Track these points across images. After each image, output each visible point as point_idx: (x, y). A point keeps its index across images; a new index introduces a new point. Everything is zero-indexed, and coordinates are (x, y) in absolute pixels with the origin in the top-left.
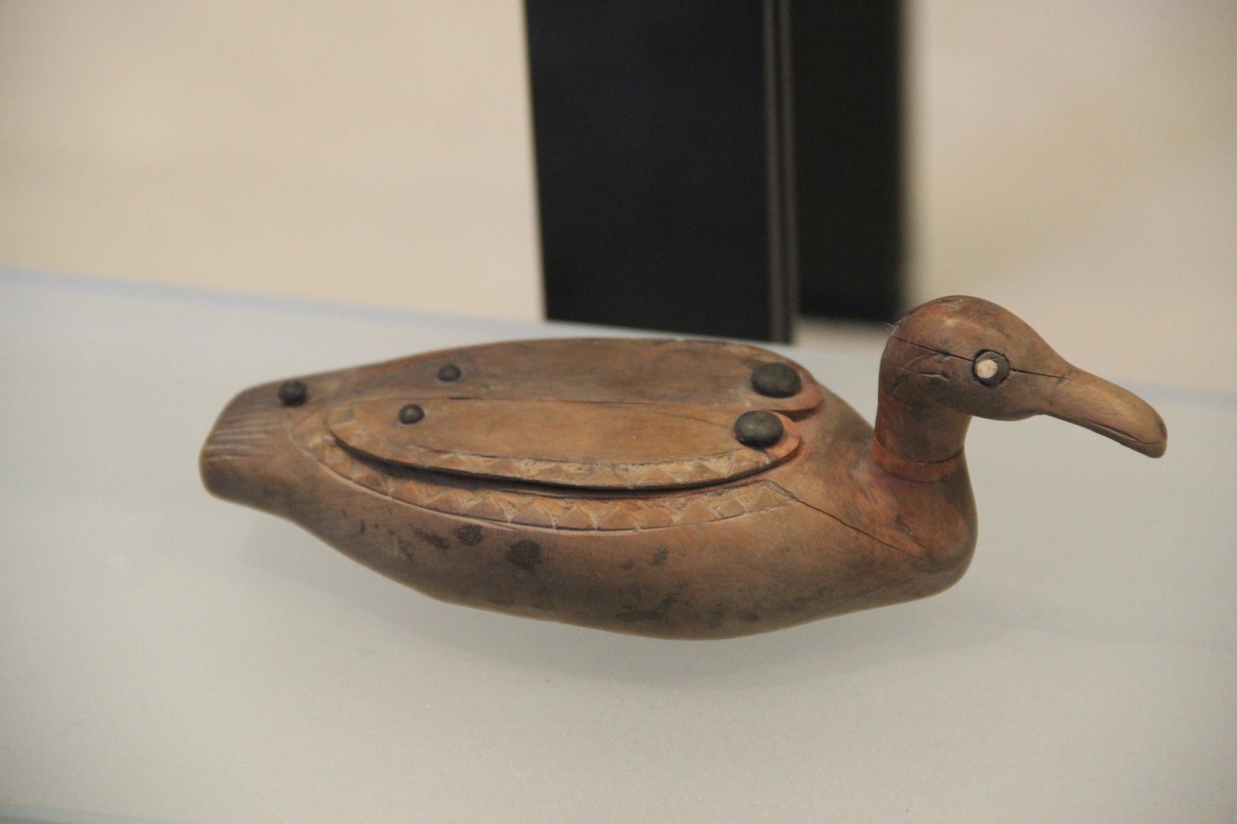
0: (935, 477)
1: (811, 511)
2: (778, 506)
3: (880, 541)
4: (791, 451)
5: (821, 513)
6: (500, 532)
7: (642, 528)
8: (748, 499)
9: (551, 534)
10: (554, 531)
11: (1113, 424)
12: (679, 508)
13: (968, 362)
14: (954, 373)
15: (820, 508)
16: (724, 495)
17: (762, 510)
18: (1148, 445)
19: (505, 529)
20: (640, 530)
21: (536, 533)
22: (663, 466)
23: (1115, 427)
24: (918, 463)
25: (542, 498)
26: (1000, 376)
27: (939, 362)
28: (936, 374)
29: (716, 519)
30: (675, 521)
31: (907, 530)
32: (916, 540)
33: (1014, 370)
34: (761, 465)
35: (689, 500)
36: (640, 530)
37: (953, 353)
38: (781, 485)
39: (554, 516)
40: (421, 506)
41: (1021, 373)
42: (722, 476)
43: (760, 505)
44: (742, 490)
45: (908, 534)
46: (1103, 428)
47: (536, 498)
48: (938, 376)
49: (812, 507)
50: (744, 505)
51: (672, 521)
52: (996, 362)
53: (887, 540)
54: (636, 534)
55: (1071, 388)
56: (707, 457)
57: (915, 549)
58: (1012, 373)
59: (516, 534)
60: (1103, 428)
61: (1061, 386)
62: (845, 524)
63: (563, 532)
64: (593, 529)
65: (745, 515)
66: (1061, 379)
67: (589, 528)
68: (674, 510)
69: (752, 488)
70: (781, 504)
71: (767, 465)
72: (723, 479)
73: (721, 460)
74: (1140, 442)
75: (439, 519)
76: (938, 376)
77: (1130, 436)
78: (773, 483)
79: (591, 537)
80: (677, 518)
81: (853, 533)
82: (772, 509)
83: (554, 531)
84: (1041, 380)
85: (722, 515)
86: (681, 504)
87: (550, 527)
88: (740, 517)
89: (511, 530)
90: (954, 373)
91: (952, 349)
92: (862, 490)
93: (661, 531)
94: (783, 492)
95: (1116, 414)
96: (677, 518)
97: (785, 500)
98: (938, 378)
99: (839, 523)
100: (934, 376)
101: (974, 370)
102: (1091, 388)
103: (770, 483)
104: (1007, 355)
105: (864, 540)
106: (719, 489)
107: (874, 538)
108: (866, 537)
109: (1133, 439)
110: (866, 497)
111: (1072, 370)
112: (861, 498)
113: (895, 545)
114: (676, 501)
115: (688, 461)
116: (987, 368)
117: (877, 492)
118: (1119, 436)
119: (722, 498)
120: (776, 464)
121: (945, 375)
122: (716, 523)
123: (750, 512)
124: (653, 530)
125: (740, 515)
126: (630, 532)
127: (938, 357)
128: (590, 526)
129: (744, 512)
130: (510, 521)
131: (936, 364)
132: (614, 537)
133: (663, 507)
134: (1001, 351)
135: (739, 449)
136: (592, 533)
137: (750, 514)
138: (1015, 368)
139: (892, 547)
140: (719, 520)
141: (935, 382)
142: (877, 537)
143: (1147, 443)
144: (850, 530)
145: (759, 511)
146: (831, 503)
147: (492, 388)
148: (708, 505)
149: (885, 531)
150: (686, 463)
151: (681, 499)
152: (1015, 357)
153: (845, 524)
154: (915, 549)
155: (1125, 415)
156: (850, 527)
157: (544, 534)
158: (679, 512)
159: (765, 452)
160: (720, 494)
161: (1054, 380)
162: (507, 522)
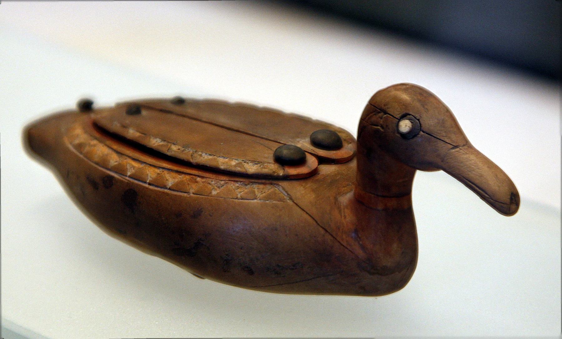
0: (380, 207)
2: (279, 201)
3: (339, 242)
5: (305, 213)
7: (193, 194)
10: (147, 186)
11: (477, 182)
12: (219, 187)
13: (396, 119)
14: (387, 126)
16: (249, 186)
18: (497, 203)
20: (192, 195)
21: (137, 185)
22: (221, 158)
23: (478, 185)
26: (413, 134)
27: (381, 118)
28: (378, 126)
29: (237, 198)
30: (213, 194)
31: (359, 240)
32: (363, 247)
33: (423, 132)
34: (276, 174)
35: (226, 183)
37: (390, 113)
40: (92, 162)
41: (427, 135)
43: (268, 198)
44: (261, 186)
45: (359, 243)
46: (470, 184)
48: (379, 127)
49: (300, 208)
50: (259, 195)
51: (211, 193)
52: (412, 122)
53: (345, 244)
54: (188, 196)
55: (461, 155)
56: (248, 161)
57: (361, 253)
58: (421, 133)
59: (129, 184)
60: (470, 184)
62: (319, 224)
63: (151, 187)
64: (166, 188)
65: (255, 201)
68: (216, 187)
69: (268, 187)
70: (281, 200)
73: (256, 165)
74: (492, 199)
76: (379, 127)
77: (486, 193)
78: (282, 187)
79: (164, 193)
80: (214, 193)
81: (322, 232)
82: (274, 202)
83: (147, 186)
84: (441, 144)
86: (221, 184)
87: (145, 182)
88: (252, 201)
90: (387, 126)
91: (389, 110)
92: (339, 208)
93: (203, 198)
95: (481, 176)
96: (214, 193)
98: (379, 129)
99: (314, 223)
100: (376, 127)
101: (398, 125)
102: (472, 157)
104: (420, 120)
105: (328, 238)
109: (487, 196)
111: (467, 143)
113: (349, 247)
114: (218, 182)
115: (235, 160)
116: (405, 126)
118: (479, 192)
119: (246, 187)
120: (287, 178)
122: (236, 200)
123: (260, 199)
124: (199, 196)
125: (253, 200)
126: (185, 195)
128: (165, 186)
129: (256, 199)
130: (128, 176)
131: (379, 119)
133: (210, 184)
134: (417, 116)
136: (166, 190)
137: (259, 201)
138: (424, 130)
139: (346, 248)
140: (238, 199)
142: (339, 239)
143: (496, 201)
144: (321, 229)
145: (266, 200)
149: (344, 237)
153: (319, 224)
154: (361, 253)
155: (493, 185)
156: (321, 227)
157: (141, 186)
158: (218, 189)
159: (284, 169)
162: (126, 176)
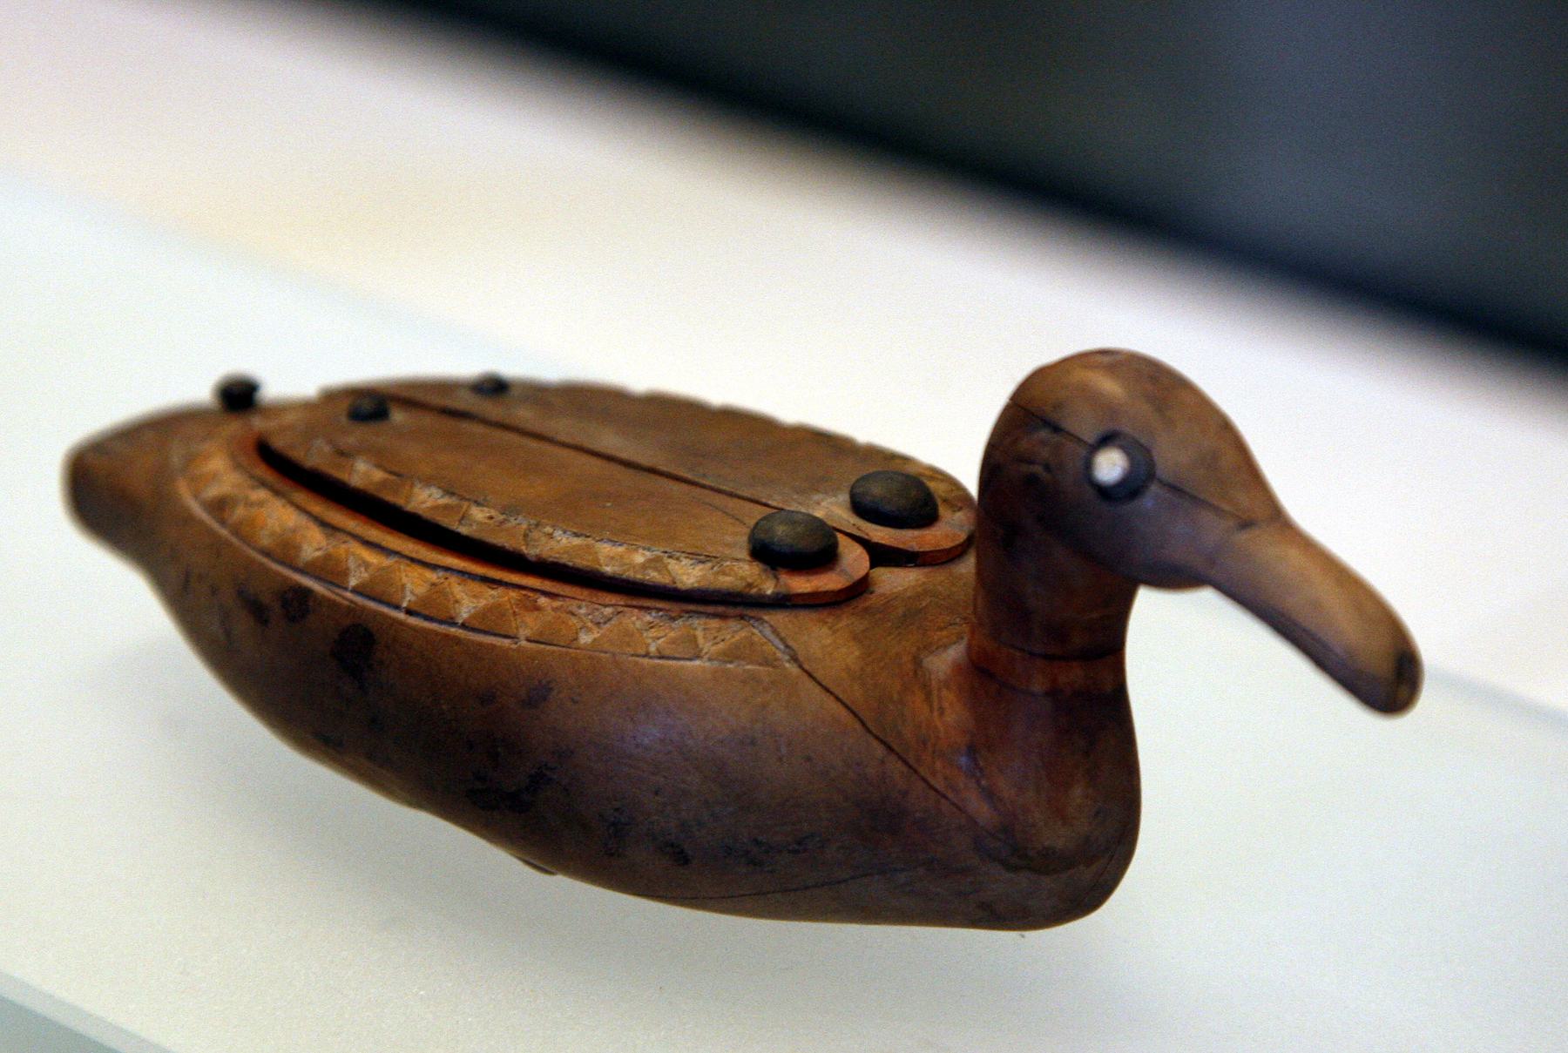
1: (818, 690)
2: (760, 664)
3: (924, 780)
4: (820, 590)
5: (832, 698)
6: (333, 605)
7: (528, 640)
8: (718, 640)
9: (395, 621)
10: (401, 616)
15: (833, 689)
16: (680, 622)
17: (731, 662)
19: (338, 599)
20: (524, 643)
24: (1011, 651)
25: (408, 562)
26: (1129, 488)
29: (647, 655)
31: (978, 774)
32: (990, 795)
36: (524, 643)
38: (783, 635)
39: (412, 592)
42: (679, 586)
43: (732, 655)
44: (714, 623)
47: (402, 560)
50: (707, 647)
53: (939, 783)
54: (514, 646)
55: (1265, 548)
56: (678, 554)
59: (352, 610)
61: (1243, 537)
62: (869, 731)
63: (412, 621)
65: (697, 662)
66: (1246, 524)
67: (451, 622)
68: (590, 624)
69: (733, 625)
70: (766, 662)
71: (764, 596)
72: (676, 590)
75: (267, 570)
78: (771, 626)
79: (447, 636)
80: (585, 639)
81: (880, 751)
82: (749, 667)
83: (401, 616)
85: (660, 652)
86: (604, 616)
87: (397, 607)
88: (688, 663)
89: (346, 603)
93: (554, 652)
94: (782, 647)
96: (585, 639)
97: (789, 661)
99: (858, 726)
103: (766, 625)
105: (895, 768)
106: (675, 608)
107: (916, 772)
108: (900, 764)
110: (928, 697)
111: (1276, 516)
112: (918, 698)
113: (950, 795)
114: (597, 609)
115: (644, 549)
116: (1110, 466)
117: (949, 696)
119: (673, 625)
121: (1047, 468)
122: (646, 661)
125: (690, 659)
126: (506, 642)
127: (1044, 434)
129: (698, 657)
130: (350, 588)
132: (480, 644)
135: (744, 560)
136: (453, 630)
139: (945, 797)
140: (651, 658)
141: (1032, 480)
142: (922, 771)
144: (875, 743)
146: (856, 688)
147: (725, 565)
148: (646, 630)
150: (641, 551)
151: (608, 605)
152: (1171, 456)
153: (869, 731)
155: (1346, 630)
156: (877, 738)
158: (595, 629)
160: (673, 619)
161: (1231, 523)
162: (346, 589)
